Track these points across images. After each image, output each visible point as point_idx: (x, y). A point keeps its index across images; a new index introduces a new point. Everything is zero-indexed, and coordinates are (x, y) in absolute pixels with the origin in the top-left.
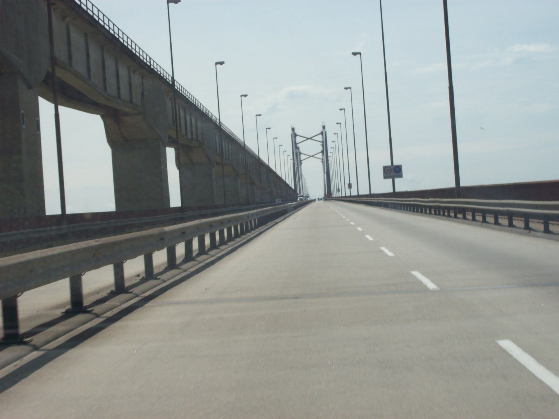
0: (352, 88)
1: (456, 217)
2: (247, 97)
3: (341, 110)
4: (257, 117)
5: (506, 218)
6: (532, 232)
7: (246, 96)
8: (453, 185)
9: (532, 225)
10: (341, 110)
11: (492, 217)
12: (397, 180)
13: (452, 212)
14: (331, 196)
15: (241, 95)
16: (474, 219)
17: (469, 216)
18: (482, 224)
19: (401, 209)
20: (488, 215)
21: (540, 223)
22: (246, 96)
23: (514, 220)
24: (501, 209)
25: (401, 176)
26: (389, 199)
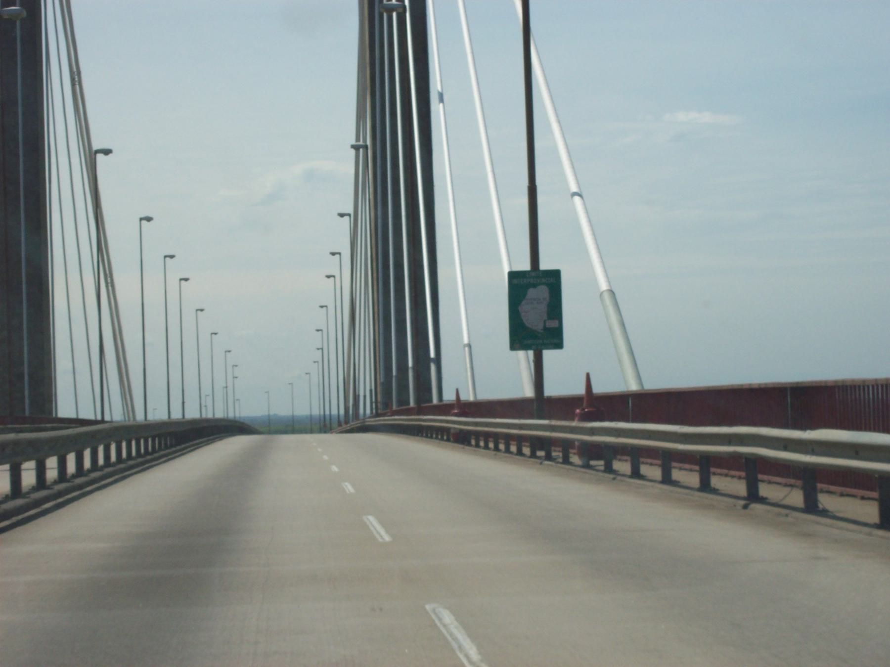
0: (342, 255)
1: (533, 455)
2: (174, 259)
3: (333, 254)
4: (168, 259)
5: (797, 487)
6: (619, 478)
7: (172, 257)
8: (528, 392)
9: (676, 475)
10: (333, 254)
11: (740, 478)
12: (548, 355)
13: (525, 446)
14: (817, 507)
15: (148, 223)
16: (508, 450)
17: (557, 453)
18: (745, 507)
19: (431, 437)
20: (765, 477)
21: (869, 499)
22: (172, 257)
23: (714, 474)
24: (681, 447)
25: (559, 345)
26: (554, 422)
